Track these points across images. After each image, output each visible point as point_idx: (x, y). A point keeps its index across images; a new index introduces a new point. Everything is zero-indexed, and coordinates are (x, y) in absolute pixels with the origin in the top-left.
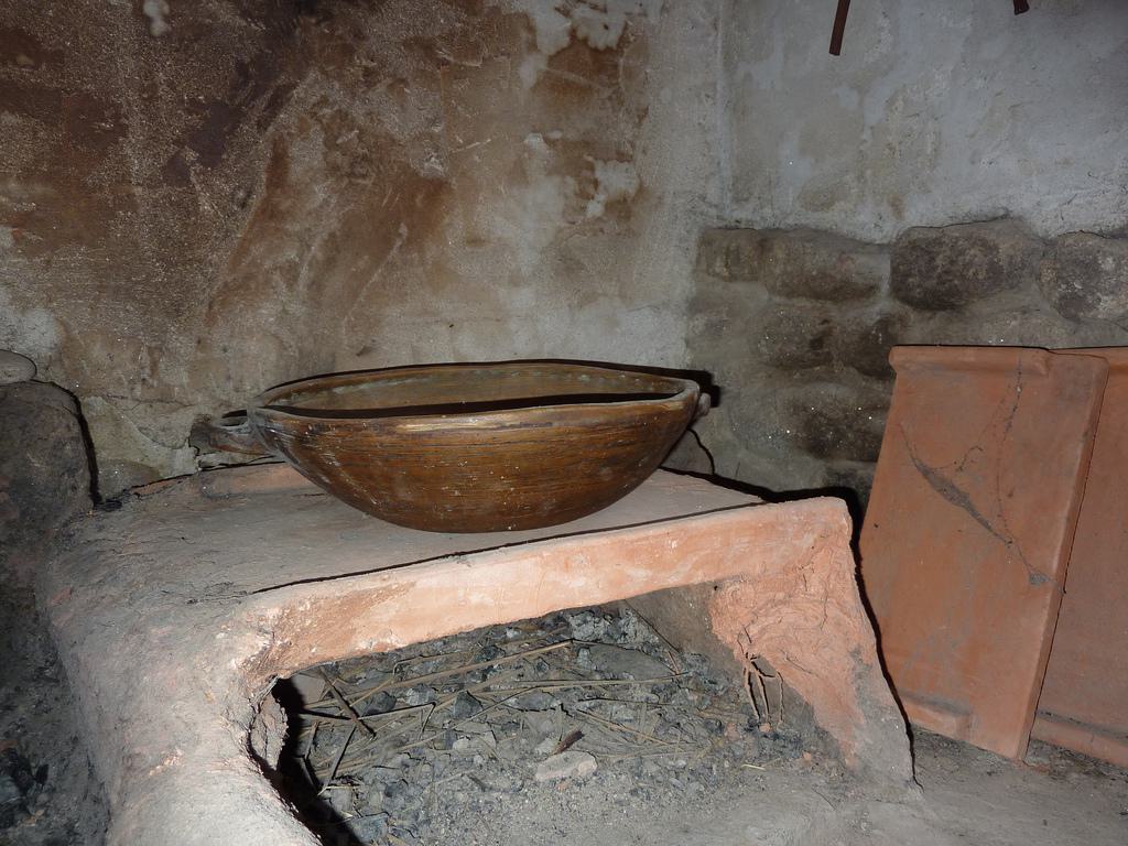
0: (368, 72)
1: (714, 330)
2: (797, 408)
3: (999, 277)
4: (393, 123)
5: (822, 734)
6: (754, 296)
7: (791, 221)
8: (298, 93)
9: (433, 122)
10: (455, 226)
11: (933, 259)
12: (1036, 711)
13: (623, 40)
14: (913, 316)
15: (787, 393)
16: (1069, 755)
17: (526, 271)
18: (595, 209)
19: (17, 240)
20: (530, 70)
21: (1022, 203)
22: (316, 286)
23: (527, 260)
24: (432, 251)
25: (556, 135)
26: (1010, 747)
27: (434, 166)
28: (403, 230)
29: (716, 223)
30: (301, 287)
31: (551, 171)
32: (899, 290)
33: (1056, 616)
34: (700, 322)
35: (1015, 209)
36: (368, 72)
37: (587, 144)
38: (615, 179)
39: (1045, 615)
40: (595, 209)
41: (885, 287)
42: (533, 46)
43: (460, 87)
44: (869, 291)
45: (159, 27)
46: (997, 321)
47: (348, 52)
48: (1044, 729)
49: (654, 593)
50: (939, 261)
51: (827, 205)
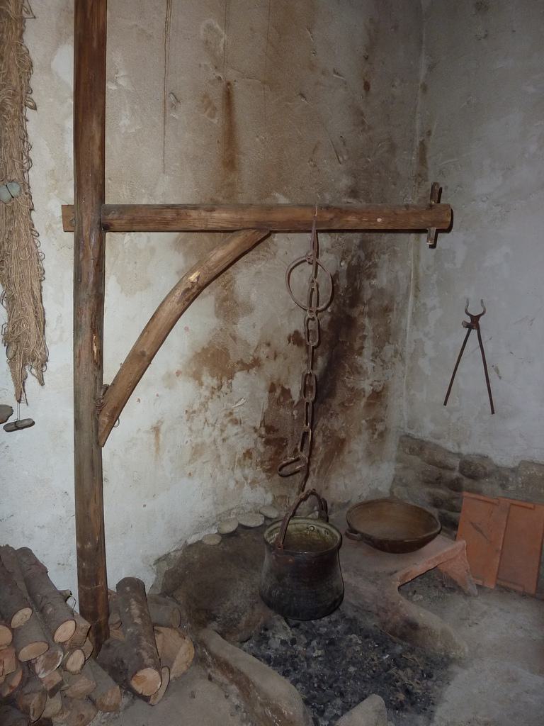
0: (332, 414)
1: (405, 468)
2: (430, 494)
3: (487, 475)
4: (336, 427)
5: (459, 587)
6: (417, 460)
7: (427, 439)
8: (319, 424)
9: (343, 423)
10: (346, 449)
11: (470, 467)
12: (497, 578)
13: (383, 388)
14: (464, 478)
15: (427, 489)
16: (502, 587)
17: (360, 457)
18: (375, 436)
19: (267, 476)
20: (363, 402)
21: (491, 455)
22: (319, 472)
23: (361, 454)
24: (341, 457)
25: (368, 419)
26: (492, 586)
27: (343, 435)
28: (336, 453)
29: (403, 434)
30: (316, 474)
31: (367, 429)
32: (461, 471)
33: (501, 559)
34: (400, 465)
35: (490, 456)
36: (332, 414)
37: (374, 420)
38: (380, 427)
39: (499, 558)
40: (375, 436)
41: (458, 468)
42: (364, 396)
43: (348, 412)
44: (452, 469)
45: (296, 417)
46: (487, 486)
47: (328, 410)
48: (498, 582)
49: (403, 553)
50: (472, 468)
51: (439, 439)
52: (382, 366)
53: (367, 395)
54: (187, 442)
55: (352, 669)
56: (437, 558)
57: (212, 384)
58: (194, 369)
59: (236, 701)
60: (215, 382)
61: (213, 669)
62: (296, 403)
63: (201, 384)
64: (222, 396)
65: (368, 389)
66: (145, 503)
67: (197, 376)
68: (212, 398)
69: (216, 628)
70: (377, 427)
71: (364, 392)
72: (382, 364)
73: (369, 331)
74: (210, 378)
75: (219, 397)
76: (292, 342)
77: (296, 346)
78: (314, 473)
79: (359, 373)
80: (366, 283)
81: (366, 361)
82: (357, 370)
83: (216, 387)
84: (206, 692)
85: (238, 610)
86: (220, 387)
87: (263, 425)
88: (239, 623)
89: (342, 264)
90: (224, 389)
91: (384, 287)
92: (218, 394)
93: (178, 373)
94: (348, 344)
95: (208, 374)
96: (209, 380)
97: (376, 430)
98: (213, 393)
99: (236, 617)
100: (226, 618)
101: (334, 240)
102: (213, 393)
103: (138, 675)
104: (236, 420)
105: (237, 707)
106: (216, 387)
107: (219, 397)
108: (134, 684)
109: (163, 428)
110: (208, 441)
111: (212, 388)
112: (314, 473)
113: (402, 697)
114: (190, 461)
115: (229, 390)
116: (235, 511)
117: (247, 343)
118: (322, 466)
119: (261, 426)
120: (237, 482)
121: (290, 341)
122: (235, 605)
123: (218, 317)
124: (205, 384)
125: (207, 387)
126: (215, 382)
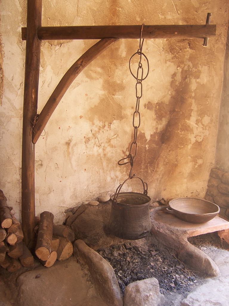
22: (160, 181)
25: (192, 156)
30: (158, 181)
37: (196, 157)
42: (190, 143)
52: (202, 128)
53: (192, 143)
54: (84, 153)
55: (152, 270)
56: (214, 228)
57: (99, 125)
58: (90, 116)
59: (86, 272)
60: (101, 124)
61: (79, 257)
62: (148, 141)
63: (93, 124)
64: (105, 131)
65: (193, 140)
66: (61, 183)
67: (91, 120)
68: (99, 132)
69: (86, 242)
70: (197, 161)
71: (190, 141)
72: (202, 126)
73: (194, 107)
74: (98, 121)
75: (103, 132)
76: (147, 108)
77: (149, 110)
78: (157, 181)
79: (187, 130)
80: (193, 80)
81: (192, 123)
82: (187, 129)
83: (102, 127)
84: (74, 265)
85: (99, 235)
86: (104, 126)
87: (127, 150)
88: (98, 241)
89: (178, 68)
90: (106, 128)
91: (205, 84)
92: (103, 130)
93: (81, 117)
94: (181, 113)
95: (97, 119)
96: (98, 123)
97: (197, 163)
98: (99, 129)
99: (97, 238)
100: (92, 238)
101: (173, 55)
102: (99, 129)
103: (38, 249)
104: (112, 145)
105: (86, 274)
106: (102, 127)
107: (103, 132)
108: (37, 253)
109: (72, 144)
110: (96, 154)
111: (100, 127)
112: (157, 181)
113: (173, 285)
114: (85, 163)
115: (109, 129)
116: (109, 193)
117: (120, 105)
118: (162, 178)
119: (126, 151)
120: (112, 178)
121: (145, 108)
122: (97, 232)
123: (104, 91)
124: (96, 124)
125: (97, 126)
126: (101, 124)
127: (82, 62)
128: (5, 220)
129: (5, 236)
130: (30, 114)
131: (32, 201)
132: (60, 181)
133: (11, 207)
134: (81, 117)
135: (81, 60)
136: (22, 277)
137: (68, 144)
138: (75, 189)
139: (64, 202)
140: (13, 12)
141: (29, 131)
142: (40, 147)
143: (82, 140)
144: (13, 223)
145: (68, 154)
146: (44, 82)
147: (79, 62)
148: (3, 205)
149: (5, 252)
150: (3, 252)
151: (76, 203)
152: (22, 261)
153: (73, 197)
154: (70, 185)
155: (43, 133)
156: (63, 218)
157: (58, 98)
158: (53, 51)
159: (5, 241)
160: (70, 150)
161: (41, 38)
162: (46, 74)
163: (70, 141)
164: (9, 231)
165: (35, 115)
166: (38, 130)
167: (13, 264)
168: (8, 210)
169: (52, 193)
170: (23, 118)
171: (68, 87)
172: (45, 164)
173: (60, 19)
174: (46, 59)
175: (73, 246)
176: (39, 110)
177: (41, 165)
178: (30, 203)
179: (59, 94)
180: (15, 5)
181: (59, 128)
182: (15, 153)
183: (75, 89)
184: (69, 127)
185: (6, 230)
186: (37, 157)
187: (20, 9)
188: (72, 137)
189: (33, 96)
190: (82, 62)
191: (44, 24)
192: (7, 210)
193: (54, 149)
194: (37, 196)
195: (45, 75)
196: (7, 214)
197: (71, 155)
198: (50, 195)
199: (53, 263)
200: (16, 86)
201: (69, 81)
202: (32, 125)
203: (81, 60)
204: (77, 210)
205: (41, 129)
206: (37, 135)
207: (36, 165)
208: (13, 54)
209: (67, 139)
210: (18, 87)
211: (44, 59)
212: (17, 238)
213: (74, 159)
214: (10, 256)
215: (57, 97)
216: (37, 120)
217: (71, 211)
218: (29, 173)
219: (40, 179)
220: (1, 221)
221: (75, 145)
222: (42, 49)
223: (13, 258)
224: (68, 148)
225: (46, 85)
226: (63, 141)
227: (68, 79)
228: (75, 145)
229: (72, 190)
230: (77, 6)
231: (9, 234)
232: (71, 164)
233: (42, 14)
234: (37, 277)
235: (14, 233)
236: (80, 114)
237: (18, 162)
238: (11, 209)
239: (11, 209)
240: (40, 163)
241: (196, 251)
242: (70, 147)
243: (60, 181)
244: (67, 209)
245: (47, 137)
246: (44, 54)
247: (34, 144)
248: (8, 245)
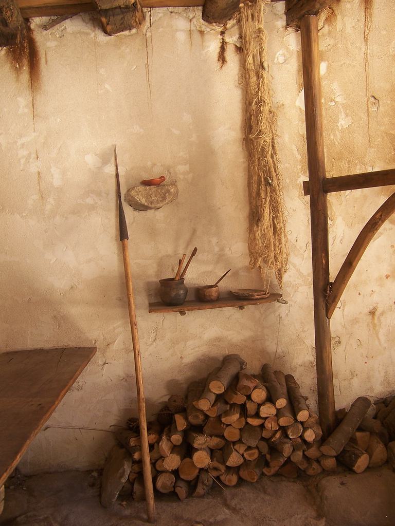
93: (387, 277)
109: (377, 313)
127: (381, 216)
128: (301, 412)
129: (301, 431)
130: (321, 284)
131: (330, 390)
132: (366, 363)
133: (306, 397)
134: (387, 277)
135: (379, 214)
136: (324, 482)
137: (372, 313)
138: (386, 372)
139: (372, 389)
140: (291, 163)
141: (322, 305)
142: (337, 320)
143: (391, 307)
144: (310, 416)
145: (374, 327)
146: (334, 239)
147: (378, 216)
148: (297, 394)
149: (302, 451)
150: (300, 451)
151: (388, 392)
152: (322, 462)
153: (384, 384)
154: (379, 367)
155: (339, 305)
156: (386, 389)
157: (355, 262)
158: (343, 198)
159: (302, 437)
160: (376, 321)
161: (327, 191)
162: (336, 228)
163: (375, 309)
164: (305, 426)
165: (328, 285)
166: (333, 302)
167: (312, 465)
168: (303, 400)
169: (355, 378)
170: (313, 285)
171: (366, 247)
172: (343, 340)
173: (348, 156)
174: (335, 210)
175: (387, 449)
176: (332, 280)
177: (339, 342)
178: (329, 392)
179: (356, 257)
180: (293, 154)
181: (359, 294)
182: (306, 329)
183: (376, 241)
184: (372, 291)
185: (302, 423)
186: (333, 334)
187: (299, 157)
188: (378, 303)
189: (324, 262)
190: (381, 216)
191: (329, 175)
192: (302, 400)
193: (355, 321)
194: (335, 382)
195: (335, 230)
196: (302, 405)
197: (377, 328)
198: (353, 380)
199: (364, 469)
200: (301, 248)
201: (367, 240)
202: (325, 297)
203: (379, 214)
204: (391, 402)
205: (336, 301)
206: (331, 309)
207: (333, 342)
208: (294, 210)
209: (371, 307)
210: (304, 248)
211: (333, 210)
212: (315, 434)
213: (382, 332)
214: (308, 455)
215: (354, 261)
216: (330, 291)
217: (384, 402)
218: (325, 355)
219: (339, 359)
220: (296, 413)
221: (382, 314)
222: (328, 198)
223: (311, 458)
224: (373, 318)
225: (337, 241)
226: (366, 310)
227: (365, 237)
228: (382, 314)
229: (383, 374)
230: (367, 134)
231: (305, 429)
232: (379, 339)
233: (325, 156)
234: (342, 484)
235: (311, 428)
236: (385, 273)
237: (311, 341)
238: (306, 399)
239: (306, 399)
240: (337, 339)
241: (151, 492)
242: (376, 318)
243: (366, 363)
244: (377, 399)
245: (344, 306)
246: (332, 204)
247: (329, 319)
248: (305, 441)
